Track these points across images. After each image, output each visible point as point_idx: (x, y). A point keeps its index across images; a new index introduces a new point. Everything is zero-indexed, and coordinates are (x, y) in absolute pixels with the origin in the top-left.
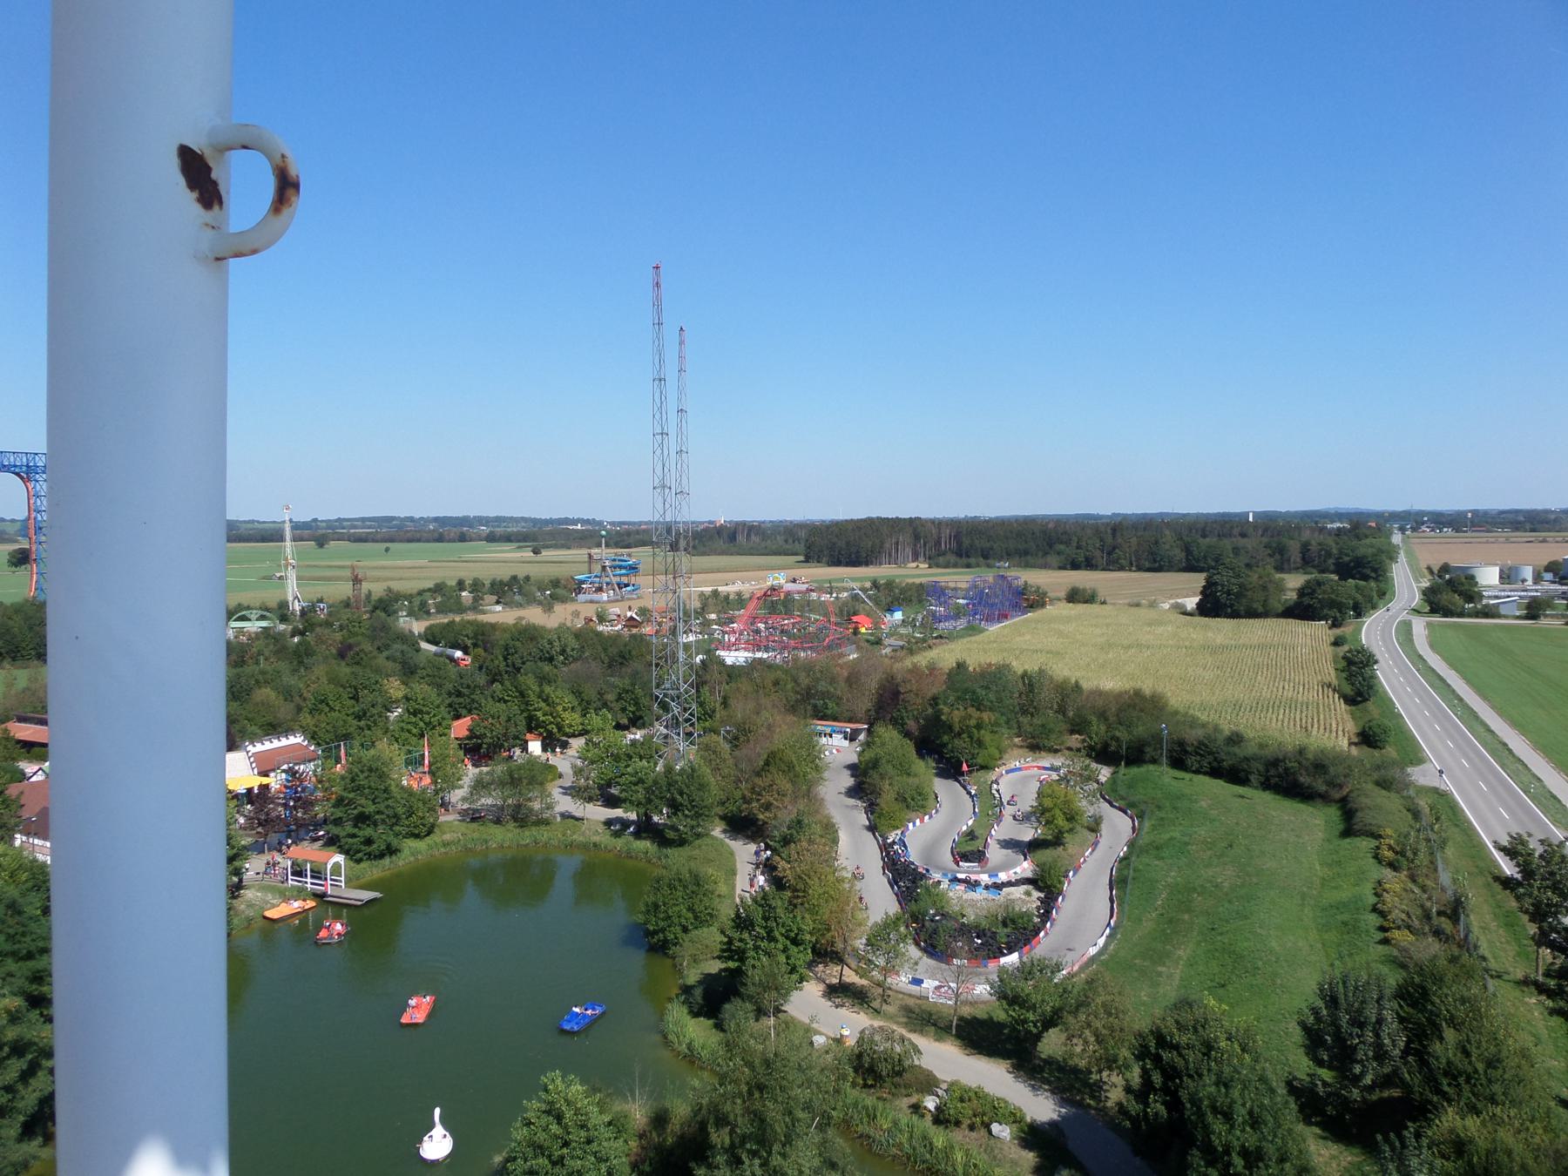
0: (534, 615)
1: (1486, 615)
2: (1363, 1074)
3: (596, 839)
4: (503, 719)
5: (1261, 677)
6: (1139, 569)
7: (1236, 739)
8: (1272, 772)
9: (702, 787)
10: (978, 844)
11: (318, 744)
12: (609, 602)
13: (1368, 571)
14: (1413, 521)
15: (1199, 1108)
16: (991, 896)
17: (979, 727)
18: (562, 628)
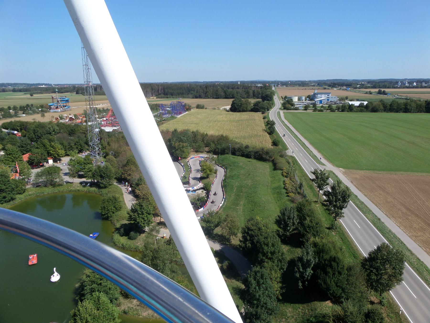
0: (38, 118)
1: (296, 110)
2: (290, 229)
3: (78, 188)
5: (245, 128)
6: (213, 98)
7: (247, 147)
8: (256, 155)
9: (110, 171)
10: (187, 180)
12: (61, 112)
13: (269, 98)
14: (277, 84)
15: (261, 244)
16: (193, 193)
17: (183, 147)
18: (50, 123)
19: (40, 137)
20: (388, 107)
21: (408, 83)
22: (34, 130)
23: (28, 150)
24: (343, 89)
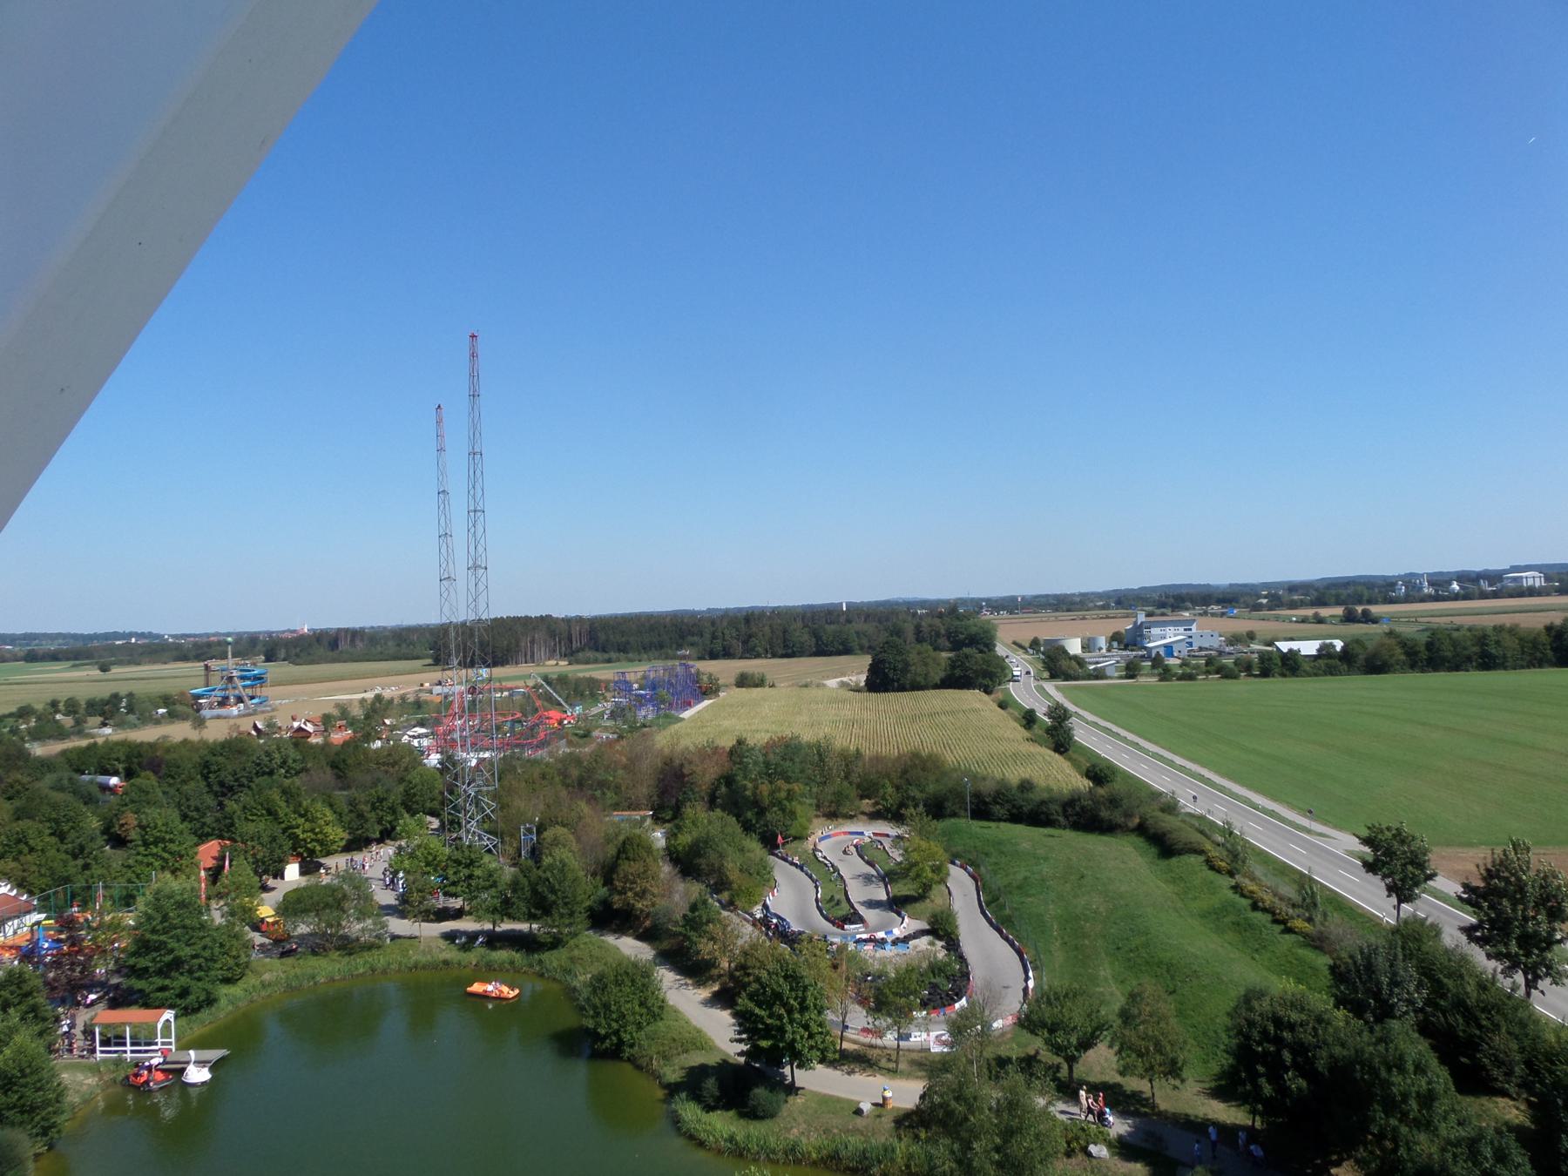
1: (1097, 678)
4: (265, 839)
6: (774, 656)
7: (1026, 786)
11: (31, 893)
12: (239, 716)
14: (1010, 606)
19: (231, 789)
20: (1424, 655)
21: (1431, 584)
22: (206, 765)
23: (206, 830)
24: (1213, 615)
